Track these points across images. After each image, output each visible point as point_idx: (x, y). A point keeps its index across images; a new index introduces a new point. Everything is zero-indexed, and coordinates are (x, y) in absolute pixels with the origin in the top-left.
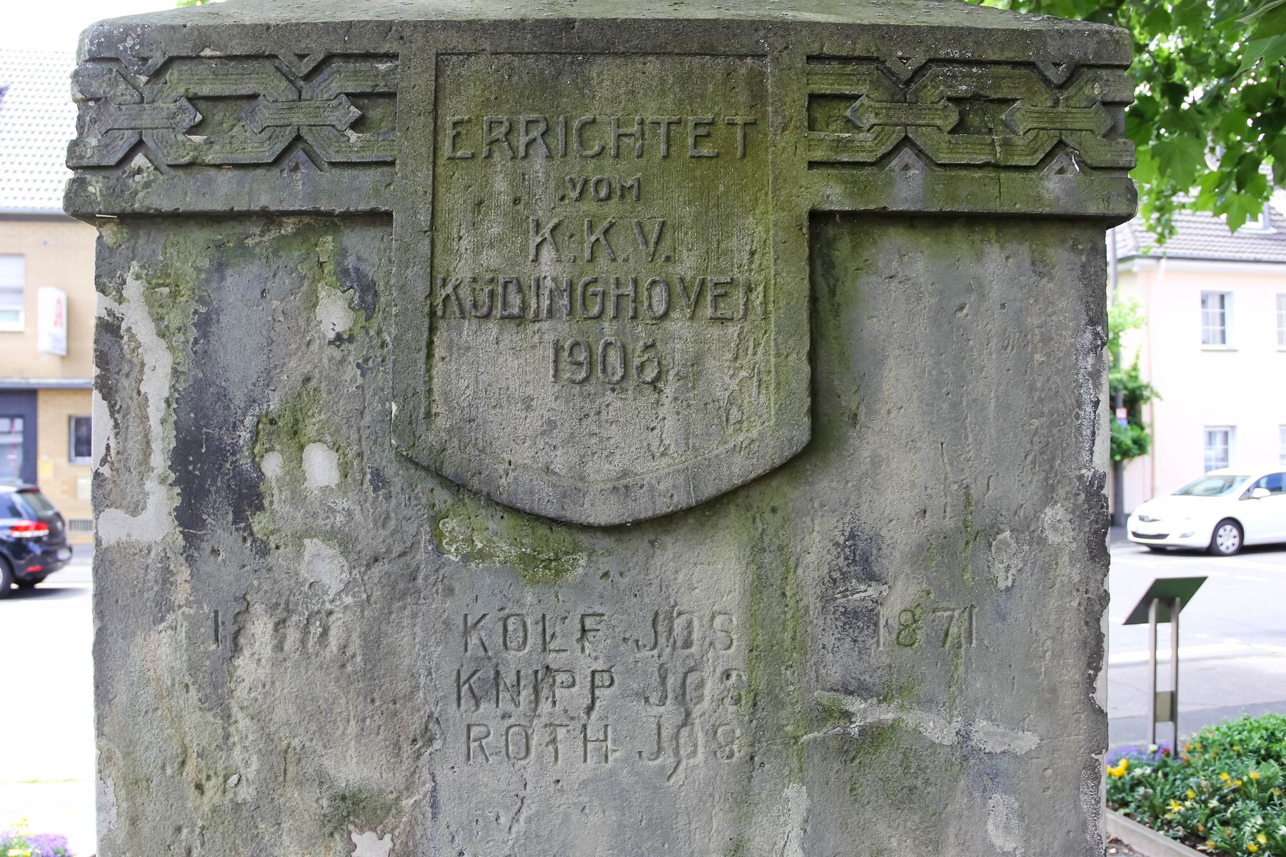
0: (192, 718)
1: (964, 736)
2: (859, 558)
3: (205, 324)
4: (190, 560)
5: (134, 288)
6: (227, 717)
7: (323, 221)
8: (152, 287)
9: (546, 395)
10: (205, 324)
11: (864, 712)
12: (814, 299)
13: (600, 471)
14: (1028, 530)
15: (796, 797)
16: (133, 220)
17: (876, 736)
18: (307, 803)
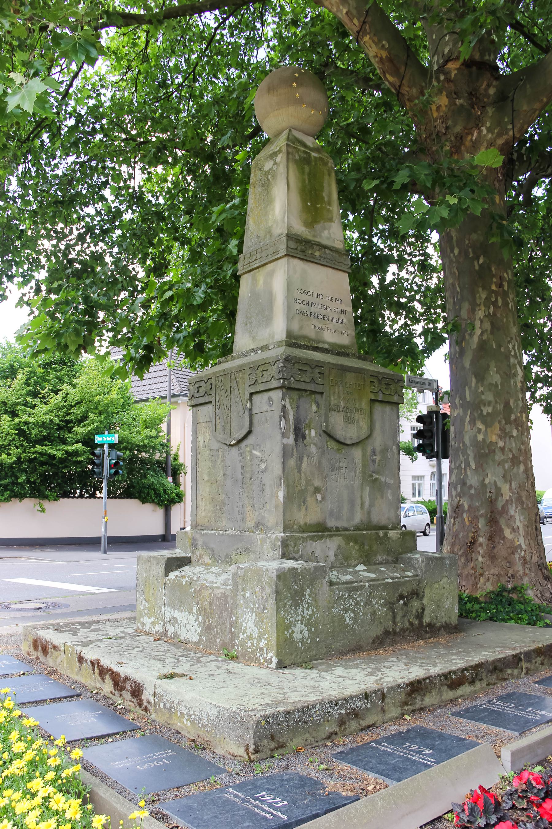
0: (296, 474)
2: (374, 453)
3: (298, 407)
5: (288, 400)
7: (314, 392)
9: (342, 423)
10: (298, 407)
11: (375, 476)
14: (391, 449)
15: (368, 488)
16: (289, 389)
17: (376, 479)
18: (311, 489)
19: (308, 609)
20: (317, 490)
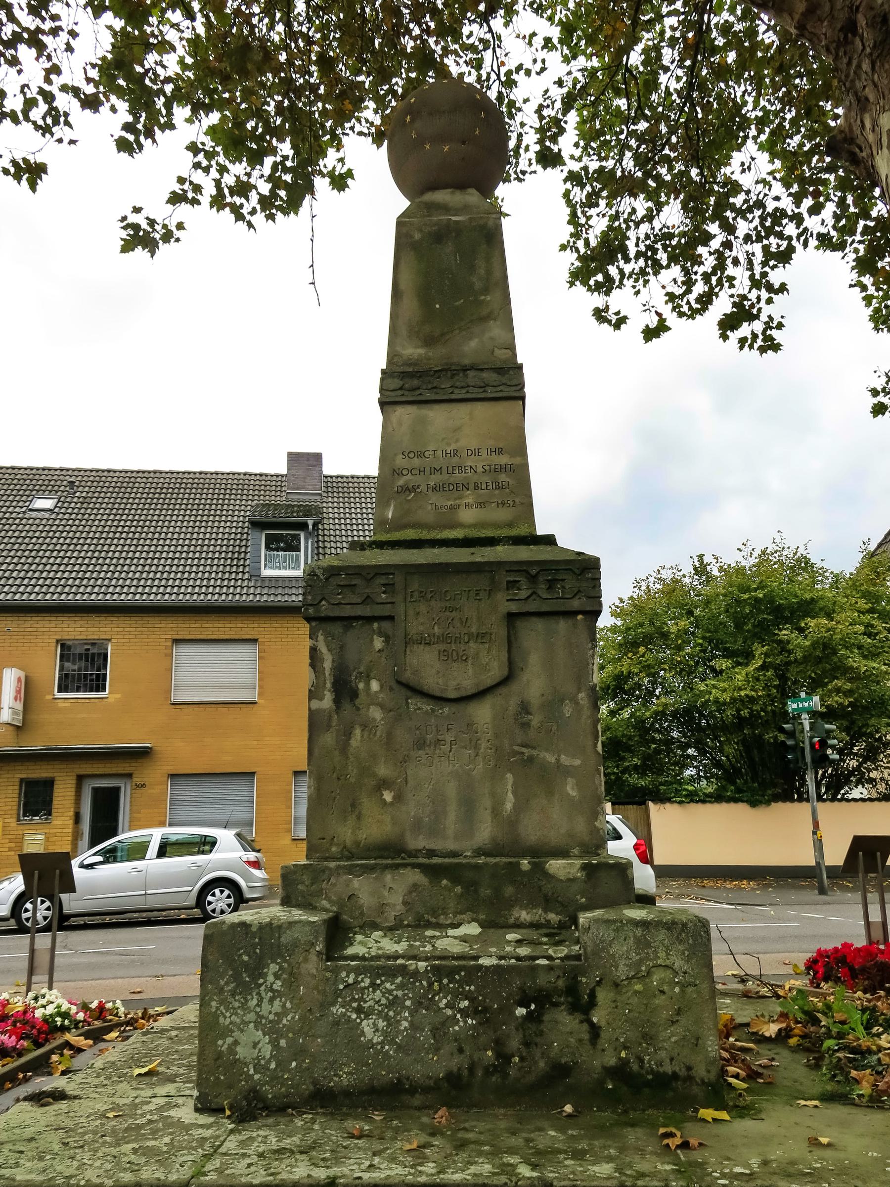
1: (558, 760)
3: (342, 647)
4: (337, 713)
5: (321, 638)
6: (347, 758)
8: (326, 637)
10: (342, 647)
12: (509, 637)
13: (453, 684)
15: (509, 777)
17: (531, 759)
19: (271, 1000)
20: (384, 784)
